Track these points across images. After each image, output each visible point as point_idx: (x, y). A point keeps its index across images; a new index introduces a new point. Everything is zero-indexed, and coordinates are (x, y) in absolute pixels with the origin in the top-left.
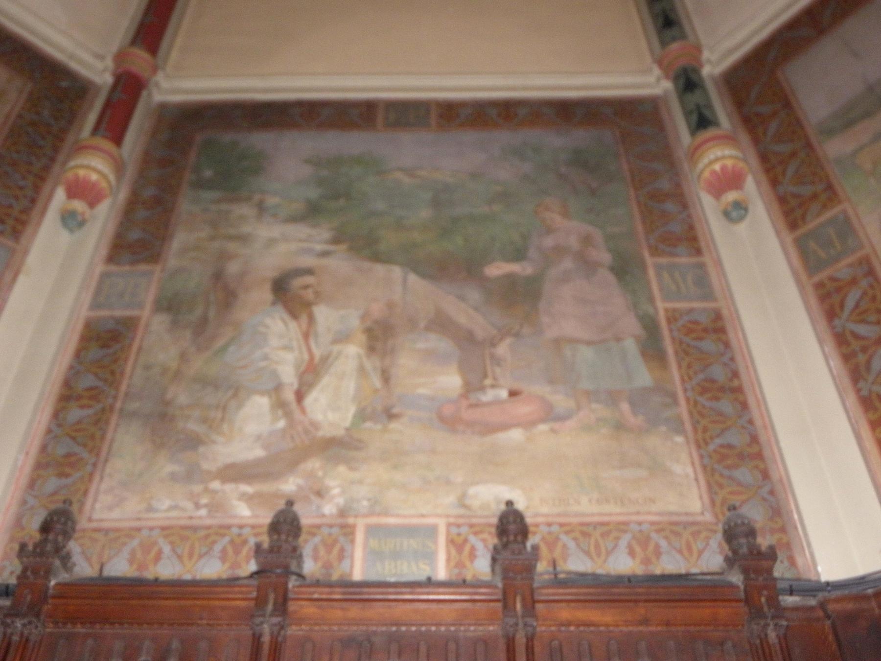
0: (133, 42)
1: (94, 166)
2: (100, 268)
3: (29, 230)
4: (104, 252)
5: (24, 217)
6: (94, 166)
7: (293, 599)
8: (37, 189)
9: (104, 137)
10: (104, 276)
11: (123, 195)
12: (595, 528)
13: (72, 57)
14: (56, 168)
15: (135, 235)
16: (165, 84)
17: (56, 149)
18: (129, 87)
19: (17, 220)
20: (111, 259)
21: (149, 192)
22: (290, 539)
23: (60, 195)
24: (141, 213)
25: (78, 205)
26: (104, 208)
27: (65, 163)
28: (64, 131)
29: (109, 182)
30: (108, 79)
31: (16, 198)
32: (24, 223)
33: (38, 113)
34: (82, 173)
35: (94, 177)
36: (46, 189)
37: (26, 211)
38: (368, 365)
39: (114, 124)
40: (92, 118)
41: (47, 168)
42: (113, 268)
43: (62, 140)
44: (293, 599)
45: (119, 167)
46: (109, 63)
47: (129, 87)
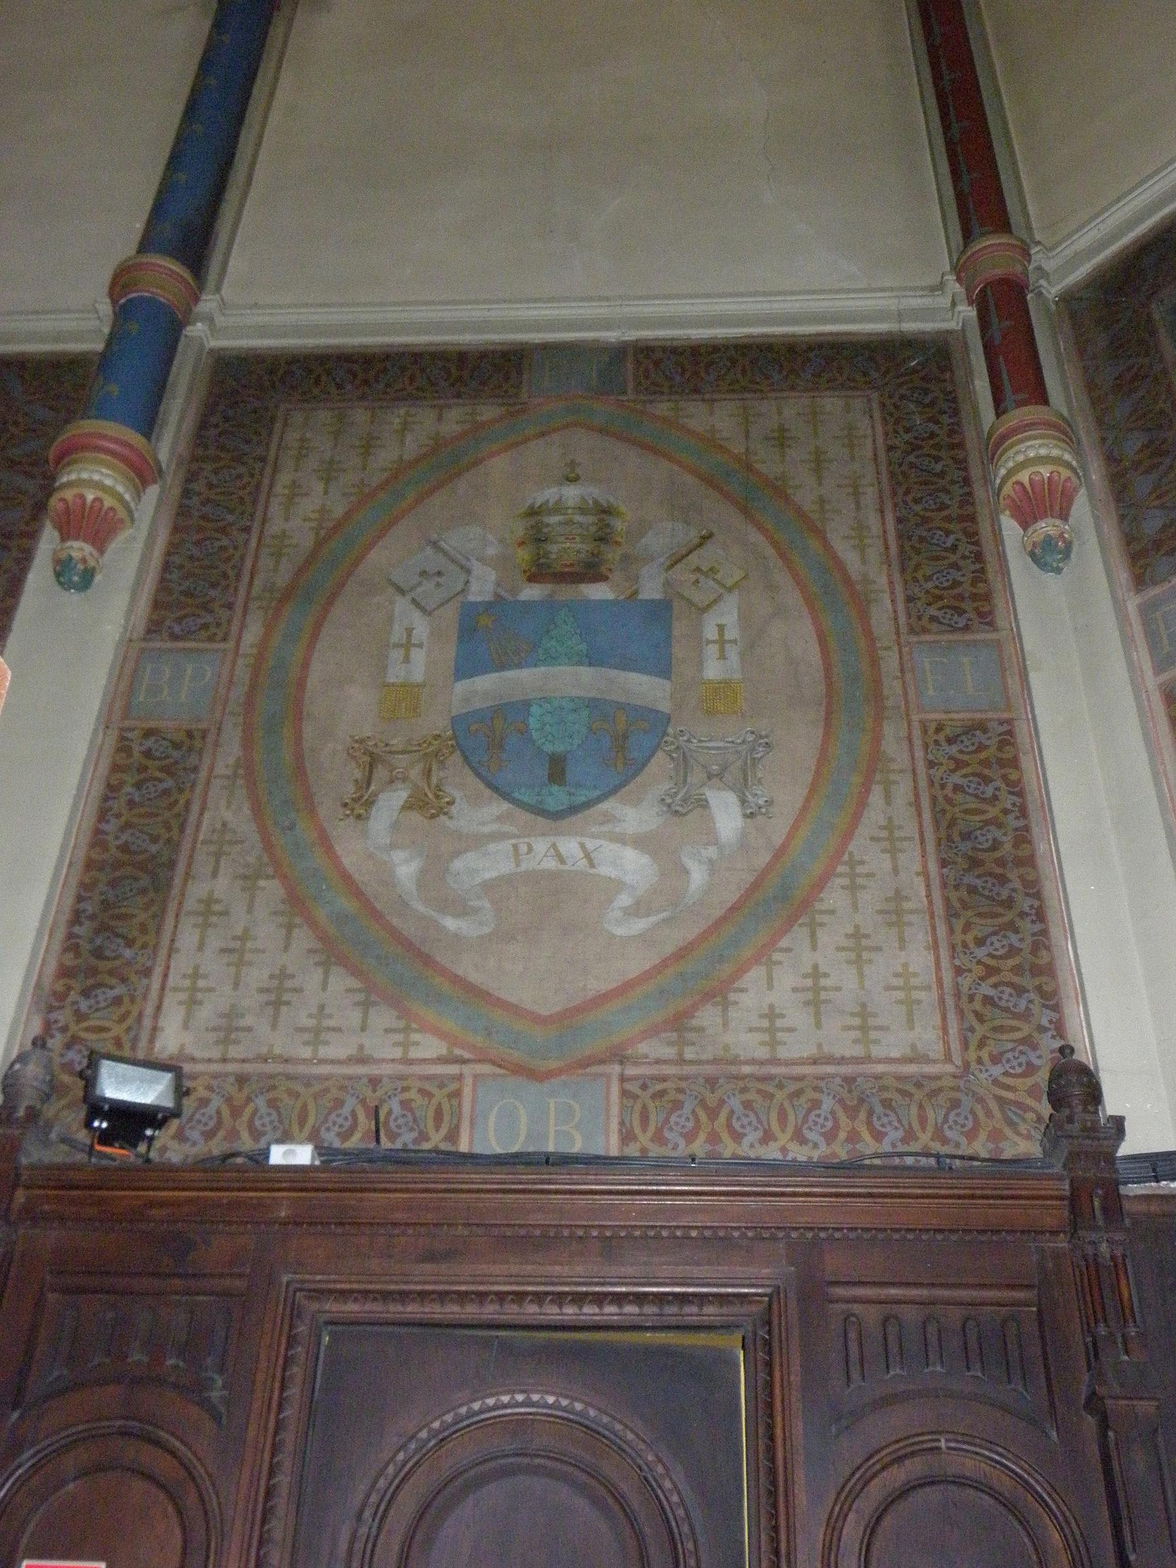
0: (968, 235)
1: (1033, 456)
2: (1132, 604)
3: (999, 602)
4: (1123, 576)
5: (981, 588)
6: (1033, 456)
7: (1061, 1198)
8: (973, 537)
9: (1020, 404)
10: (1146, 611)
11: (1097, 472)
12: (308, 1085)
13: (900, 316)
14: (979, 492)
15: (1153, 524)
16: (1049, 265)
17: (962, 464)
18: (1003, 303)
19: (974, 597)
20: (1140, 582)
21: (1134, 444)
22: (336, 1128)
23: (1009, 526)
24: (1142, 485)
25: (1046, 527)
26: (1081, 507)
27: (987, 480)
28: (955, 430)
29: (1068, 465)
30: (969, 312)
31: (955, 566)
32: (987, 597)
33: (907, 430)
34: (1024, 477)
35: (1045, 471)
36: (985, 528)
37: (980, 576)
38: (707, 396)
39: (1018, 378)
40: (982, 385)
41: (968, 499)
42: (1153, 592)
43: (961, 445)
44: (1061, 1198)
45: (1065, 432)
46: (954, 287)
47: (1003, 303)
